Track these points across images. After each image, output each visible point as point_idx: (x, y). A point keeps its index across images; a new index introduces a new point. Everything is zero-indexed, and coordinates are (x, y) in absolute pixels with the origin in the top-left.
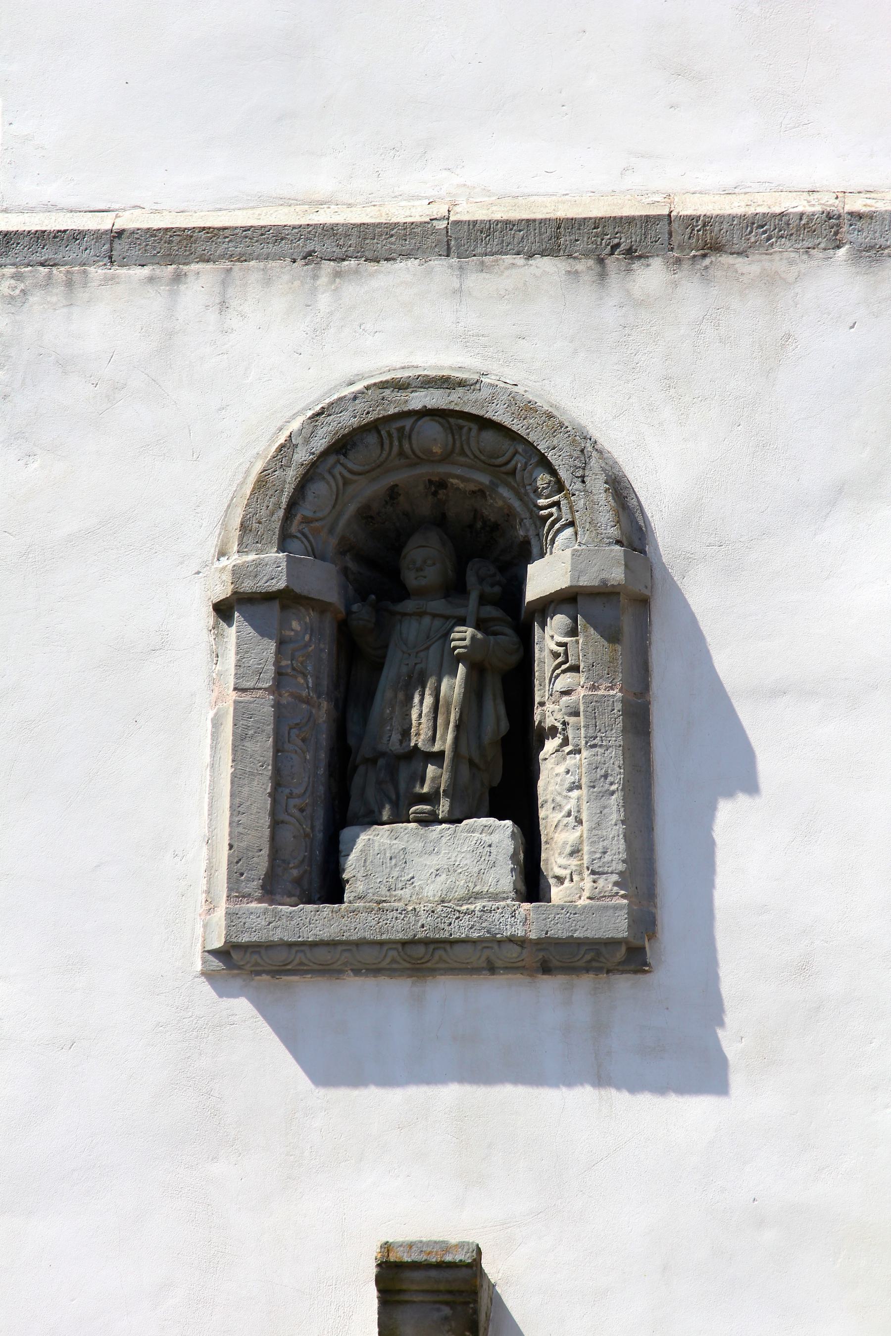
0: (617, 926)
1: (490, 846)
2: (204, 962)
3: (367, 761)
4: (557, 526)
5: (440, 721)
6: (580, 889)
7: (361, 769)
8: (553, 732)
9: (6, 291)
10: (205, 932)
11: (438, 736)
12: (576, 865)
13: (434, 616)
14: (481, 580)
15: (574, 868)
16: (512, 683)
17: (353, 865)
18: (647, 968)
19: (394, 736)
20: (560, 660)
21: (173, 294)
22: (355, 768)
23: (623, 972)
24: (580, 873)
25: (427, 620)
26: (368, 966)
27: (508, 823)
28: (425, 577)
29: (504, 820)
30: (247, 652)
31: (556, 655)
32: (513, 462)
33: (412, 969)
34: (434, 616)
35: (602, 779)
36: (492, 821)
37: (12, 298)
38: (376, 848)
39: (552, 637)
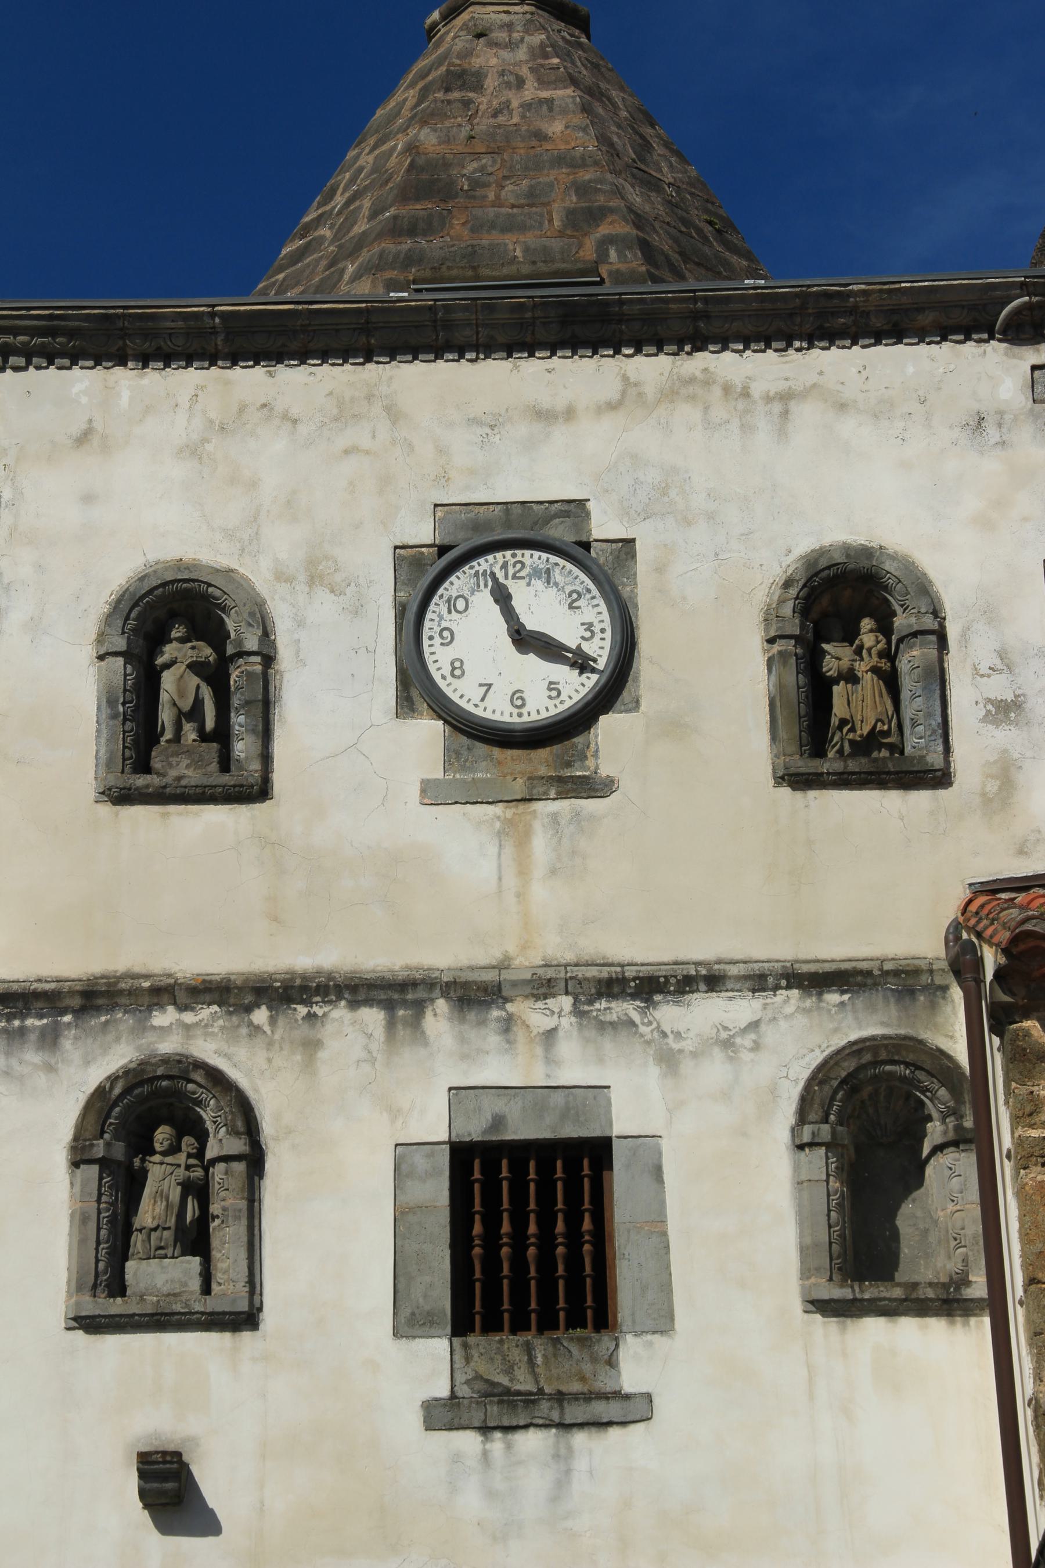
0: (243, 1306)
3: (137, 1230)
6: (230, 1289)
8: (218, 1217)
14: (188, 1146)
16: (198, 1191)
21: (309, 1065)
27: (198, 1258)
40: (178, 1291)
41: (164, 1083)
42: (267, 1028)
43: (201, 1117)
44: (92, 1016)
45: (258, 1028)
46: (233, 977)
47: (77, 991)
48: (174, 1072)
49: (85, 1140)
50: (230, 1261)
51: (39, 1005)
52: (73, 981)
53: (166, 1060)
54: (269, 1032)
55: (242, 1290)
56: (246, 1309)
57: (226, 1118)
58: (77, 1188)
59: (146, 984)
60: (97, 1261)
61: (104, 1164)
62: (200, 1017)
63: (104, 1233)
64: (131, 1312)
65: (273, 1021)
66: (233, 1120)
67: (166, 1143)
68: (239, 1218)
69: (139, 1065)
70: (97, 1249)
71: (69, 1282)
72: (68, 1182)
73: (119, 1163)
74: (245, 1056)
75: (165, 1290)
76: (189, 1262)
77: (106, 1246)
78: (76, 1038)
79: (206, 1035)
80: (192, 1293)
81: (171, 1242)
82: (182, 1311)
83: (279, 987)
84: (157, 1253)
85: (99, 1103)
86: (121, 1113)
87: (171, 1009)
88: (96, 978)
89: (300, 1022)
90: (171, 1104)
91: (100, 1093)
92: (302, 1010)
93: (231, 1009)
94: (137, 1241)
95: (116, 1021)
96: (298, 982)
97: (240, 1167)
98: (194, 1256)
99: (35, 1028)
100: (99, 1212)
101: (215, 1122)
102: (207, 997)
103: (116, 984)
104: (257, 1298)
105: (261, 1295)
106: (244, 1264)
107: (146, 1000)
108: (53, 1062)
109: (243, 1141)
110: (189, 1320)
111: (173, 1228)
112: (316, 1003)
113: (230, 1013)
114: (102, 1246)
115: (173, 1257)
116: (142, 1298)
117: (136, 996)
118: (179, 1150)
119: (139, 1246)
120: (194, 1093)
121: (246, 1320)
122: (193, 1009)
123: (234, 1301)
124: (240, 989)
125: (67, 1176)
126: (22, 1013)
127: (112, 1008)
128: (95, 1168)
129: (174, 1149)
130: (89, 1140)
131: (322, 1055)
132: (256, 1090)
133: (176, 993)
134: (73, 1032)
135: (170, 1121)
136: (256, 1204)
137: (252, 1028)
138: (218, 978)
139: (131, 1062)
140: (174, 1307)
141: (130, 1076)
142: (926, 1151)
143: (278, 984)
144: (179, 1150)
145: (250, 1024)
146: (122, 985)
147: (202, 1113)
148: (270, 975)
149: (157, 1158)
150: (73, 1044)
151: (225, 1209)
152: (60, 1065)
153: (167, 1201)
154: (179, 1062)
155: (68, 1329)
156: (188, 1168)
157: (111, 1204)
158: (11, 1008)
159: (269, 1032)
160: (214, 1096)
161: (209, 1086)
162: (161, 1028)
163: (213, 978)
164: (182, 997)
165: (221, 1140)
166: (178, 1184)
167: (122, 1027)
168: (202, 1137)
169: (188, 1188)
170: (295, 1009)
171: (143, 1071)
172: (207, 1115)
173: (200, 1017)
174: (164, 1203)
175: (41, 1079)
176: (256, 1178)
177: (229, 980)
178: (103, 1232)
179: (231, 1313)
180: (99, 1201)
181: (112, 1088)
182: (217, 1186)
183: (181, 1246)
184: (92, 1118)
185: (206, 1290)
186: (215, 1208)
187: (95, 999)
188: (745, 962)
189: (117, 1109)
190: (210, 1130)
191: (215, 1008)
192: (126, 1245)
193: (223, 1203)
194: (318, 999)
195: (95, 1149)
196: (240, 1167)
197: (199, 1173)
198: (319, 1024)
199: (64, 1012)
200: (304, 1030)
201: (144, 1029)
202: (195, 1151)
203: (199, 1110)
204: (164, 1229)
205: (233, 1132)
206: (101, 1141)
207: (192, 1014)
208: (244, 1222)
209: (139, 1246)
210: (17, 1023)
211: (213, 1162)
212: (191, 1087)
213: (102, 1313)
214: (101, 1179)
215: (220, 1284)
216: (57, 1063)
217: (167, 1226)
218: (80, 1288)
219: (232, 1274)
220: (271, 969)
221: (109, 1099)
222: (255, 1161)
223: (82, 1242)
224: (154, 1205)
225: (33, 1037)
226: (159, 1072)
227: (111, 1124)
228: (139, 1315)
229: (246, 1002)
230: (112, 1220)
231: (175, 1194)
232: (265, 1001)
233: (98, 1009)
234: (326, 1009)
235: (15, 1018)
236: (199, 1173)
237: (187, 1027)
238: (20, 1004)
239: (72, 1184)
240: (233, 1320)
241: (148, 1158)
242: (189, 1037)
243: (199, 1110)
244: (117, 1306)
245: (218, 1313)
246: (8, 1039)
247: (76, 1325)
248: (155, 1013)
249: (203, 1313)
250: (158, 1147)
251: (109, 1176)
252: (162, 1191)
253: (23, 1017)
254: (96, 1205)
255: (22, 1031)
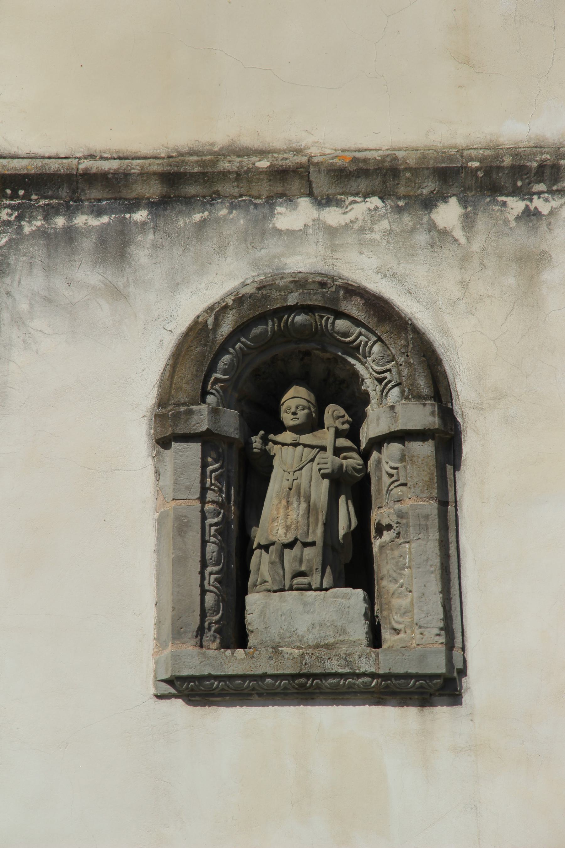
0: (437, 665)
1: (348, 607)
2: (156, 686)
3: (260, 547)
4: (390, 386)
5: (311, 520)
7: (257, 552)
8: (389, 527)
9: (5, 217)
10: (156, 667)
11: (311, 531)
12: (409, 622)
13: (305, 446)
15: (407, 624)
16: (355, 488)
17: (252, 617)
18: (458, 693)
19: (280, 532)
20: (394, 479)
21: (529, 291)
22: (252, 551)
23: (441, 695)
24: (411, 627)
25: (300, 448)
26: (268, 691)
28: (298, 419)
29: (357, 588)
30: (182, 474)
31: (391, 476)
32: (358, 341)
33: (297, 693)
34: (305, 446)
35: (425, 563)
36: (349, 590)
37: (9, 222)
38: (271, 609)
39: (387, 463)
40: (331, 640)
41: (300, 318)
42: (459, 234)
43: (355, 375)
44: (180, 212)
45: (444, 234)
46: (400, 154)
47: (155, 173)
48: (316, 300)
49: (178, 405)
50: (415, 594)
51: (95, 193)
52: (145, 158)
53: (300, 283)
54: (463, 240)
55: (434, 639)
56: (442, 670)
57: (399, 373)
58: (168, 479)
59: (264, 164)
60: (203, 592)
61: (208, 440)
62: (351, 216)
63: (211, 548)
64: (260, 671)
65: (468, 222)
66: (411, 376)
67: (302, 414)
68: (427, 528)
69: (259, 289)
70: (202, 573)
71: (159, 624)
72: (150, 470)
73: (230, 442)
74: (433, 281)
75: (311, 639)
76: (345, 596)
77: (216, 568)
78: (155, 247)
79: (362, 243)
80: (353, 644)
81: (317, 563)
82: (341, 671)
83: (478, 169)
84: (296, 582)
85: (198, 346)
86: (231, 364)
87: (304, 203)
88: (181, 154)
89: (513, 224)
90: (307, 353)
91: (198, 332)
92: (516, 205)
93: (401, 203)
94: (261, 564)
95: (217, 220)
96: (507, 161)
97: (424, 450)
98: (355, 587)
99: (90, 229)
100: (204, 518)
101: (380, 381)
102: (363, 185)
103: (214, 163)
104: (457, 654)
105: (463, 649)
106: (438, 598)
107: (264, 188)
108: (120, 283)
109: (429, 409)
110: (350, 686)
111: (320, 543)
112: (539, 194)
113: (399, 210)
114: (209, 569)
115: (321, 589)
116: (276, 650)
117: (249, 181)
118: (321, 425)
119: (265, 569)
120: (346, 334)
121: (442, 688)
122: (339, 203)
123: (422, 658)
124: (415, 171)
125: (150, 461)
126: (68, 207)
127: (213, 198)
128: (196, 448)
129: (314, 424)
130: (184, 404)
131: (550, 276)
132: (445, 332)
133: (312, 178)
134: (151, 236)
135: (304, 380)
136: (451, 508)
137: (435, 234)
138: (376, 155)
139: (244, 285)
140: (328, 664)
141: (246, 305)
142: (254, 547)
143: (476, 164)
144: (321, 425)
145: (432, 227)
146: (224, 165)
147: (358, 366)
148: (460, 151)
149: (287, 436)
150: (150, 256)
151: (401, 515)
152: (131, 289)
153: (308, 502)
154: (323, 285)
155: (160, 697)
156: (337, 451)
157: (221, 505)
158: (51, 198)
159: (463, 240)
160: (380, 339)
161: (371, 322)
162: (290, 233)
163: (369, 155)
164: (321, 184)
165: (392, 408)
166: (324, 476)
167: (228, 230)
168: (357, 405)
169: (338, 482)
170: (504, 204)
171: (265, 298)
172: (365, 372)
173: (351, 216)
174: (303, 505)
175: (103, 311)
176: (449, 468)
177: (396, 158)
178: (211, 548)
179: (418, 677)
180: (202, 499)
181: (217, 324)
182: (386, 480)
183: (333, 572)
184: (187, 372)
185: (375, 639)
186: (377, 515)
187: (184, 185)
188: (120, 158)
189: (226, 358)
190: (372, 394)
191: (375, 201)
192: (244, 572)
193: (398, 506)
194: (542, 187)
195: (195, 417)
196: (424, 450)
197: (354, 460)
198: (544, 227)
199: (134, 205)
200: (520, 237)
201: (263, 234)
202: (346, 426)
203: (350, 360)
204: (306, 545)
205: (412, 395)
206: (204, 407)
207: (339, 210)
208: (434, 534)
209: (265, 569)
210: (60, 221)
211: (378, 443)
212: (341, 324)
213: (213, 673)
214: (204, 465)
215: (397, 631)
216: (127, 285)
217: (310, 540)
218: (177, 633)
219: (418, 616)
220: (460, 141)
221: (214, 341)
222: (447, 441)
223: (179, 561)
224: (287, 508)
225: (87, 244)
226: (292, 300)
227: (217, 380)
228: (272, 676)
229: (425, 191)
230: (223, 530)
231: (321, 491)
232: (455, 190)
233: (189, 201)
234: (555, 203)
235: (57, 213)
236: (354, 460)
237: (332, 232)
238: (64, 193)
239: (157, 473)
240: (421, 687)
241: (271, 436)
242: (333, 248)
243: (350, 360)
244: (235, 662)
245: (398, 676)
246: (47, 246)
247: (173, 691)
248: (279, 209)
249: (373, 676)
250: (287, 418)
251: (216, 461)
252: (299, 487)
253: (70, 211)
254: (198, 505)
255: (70, 235)
